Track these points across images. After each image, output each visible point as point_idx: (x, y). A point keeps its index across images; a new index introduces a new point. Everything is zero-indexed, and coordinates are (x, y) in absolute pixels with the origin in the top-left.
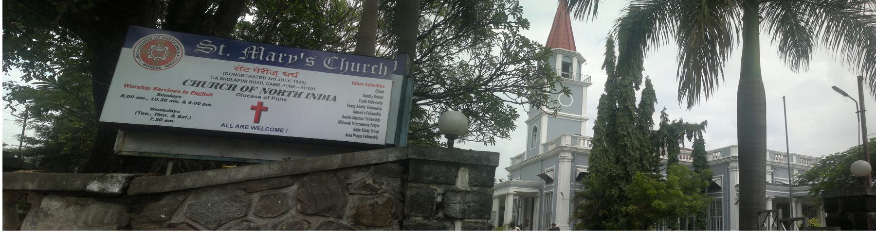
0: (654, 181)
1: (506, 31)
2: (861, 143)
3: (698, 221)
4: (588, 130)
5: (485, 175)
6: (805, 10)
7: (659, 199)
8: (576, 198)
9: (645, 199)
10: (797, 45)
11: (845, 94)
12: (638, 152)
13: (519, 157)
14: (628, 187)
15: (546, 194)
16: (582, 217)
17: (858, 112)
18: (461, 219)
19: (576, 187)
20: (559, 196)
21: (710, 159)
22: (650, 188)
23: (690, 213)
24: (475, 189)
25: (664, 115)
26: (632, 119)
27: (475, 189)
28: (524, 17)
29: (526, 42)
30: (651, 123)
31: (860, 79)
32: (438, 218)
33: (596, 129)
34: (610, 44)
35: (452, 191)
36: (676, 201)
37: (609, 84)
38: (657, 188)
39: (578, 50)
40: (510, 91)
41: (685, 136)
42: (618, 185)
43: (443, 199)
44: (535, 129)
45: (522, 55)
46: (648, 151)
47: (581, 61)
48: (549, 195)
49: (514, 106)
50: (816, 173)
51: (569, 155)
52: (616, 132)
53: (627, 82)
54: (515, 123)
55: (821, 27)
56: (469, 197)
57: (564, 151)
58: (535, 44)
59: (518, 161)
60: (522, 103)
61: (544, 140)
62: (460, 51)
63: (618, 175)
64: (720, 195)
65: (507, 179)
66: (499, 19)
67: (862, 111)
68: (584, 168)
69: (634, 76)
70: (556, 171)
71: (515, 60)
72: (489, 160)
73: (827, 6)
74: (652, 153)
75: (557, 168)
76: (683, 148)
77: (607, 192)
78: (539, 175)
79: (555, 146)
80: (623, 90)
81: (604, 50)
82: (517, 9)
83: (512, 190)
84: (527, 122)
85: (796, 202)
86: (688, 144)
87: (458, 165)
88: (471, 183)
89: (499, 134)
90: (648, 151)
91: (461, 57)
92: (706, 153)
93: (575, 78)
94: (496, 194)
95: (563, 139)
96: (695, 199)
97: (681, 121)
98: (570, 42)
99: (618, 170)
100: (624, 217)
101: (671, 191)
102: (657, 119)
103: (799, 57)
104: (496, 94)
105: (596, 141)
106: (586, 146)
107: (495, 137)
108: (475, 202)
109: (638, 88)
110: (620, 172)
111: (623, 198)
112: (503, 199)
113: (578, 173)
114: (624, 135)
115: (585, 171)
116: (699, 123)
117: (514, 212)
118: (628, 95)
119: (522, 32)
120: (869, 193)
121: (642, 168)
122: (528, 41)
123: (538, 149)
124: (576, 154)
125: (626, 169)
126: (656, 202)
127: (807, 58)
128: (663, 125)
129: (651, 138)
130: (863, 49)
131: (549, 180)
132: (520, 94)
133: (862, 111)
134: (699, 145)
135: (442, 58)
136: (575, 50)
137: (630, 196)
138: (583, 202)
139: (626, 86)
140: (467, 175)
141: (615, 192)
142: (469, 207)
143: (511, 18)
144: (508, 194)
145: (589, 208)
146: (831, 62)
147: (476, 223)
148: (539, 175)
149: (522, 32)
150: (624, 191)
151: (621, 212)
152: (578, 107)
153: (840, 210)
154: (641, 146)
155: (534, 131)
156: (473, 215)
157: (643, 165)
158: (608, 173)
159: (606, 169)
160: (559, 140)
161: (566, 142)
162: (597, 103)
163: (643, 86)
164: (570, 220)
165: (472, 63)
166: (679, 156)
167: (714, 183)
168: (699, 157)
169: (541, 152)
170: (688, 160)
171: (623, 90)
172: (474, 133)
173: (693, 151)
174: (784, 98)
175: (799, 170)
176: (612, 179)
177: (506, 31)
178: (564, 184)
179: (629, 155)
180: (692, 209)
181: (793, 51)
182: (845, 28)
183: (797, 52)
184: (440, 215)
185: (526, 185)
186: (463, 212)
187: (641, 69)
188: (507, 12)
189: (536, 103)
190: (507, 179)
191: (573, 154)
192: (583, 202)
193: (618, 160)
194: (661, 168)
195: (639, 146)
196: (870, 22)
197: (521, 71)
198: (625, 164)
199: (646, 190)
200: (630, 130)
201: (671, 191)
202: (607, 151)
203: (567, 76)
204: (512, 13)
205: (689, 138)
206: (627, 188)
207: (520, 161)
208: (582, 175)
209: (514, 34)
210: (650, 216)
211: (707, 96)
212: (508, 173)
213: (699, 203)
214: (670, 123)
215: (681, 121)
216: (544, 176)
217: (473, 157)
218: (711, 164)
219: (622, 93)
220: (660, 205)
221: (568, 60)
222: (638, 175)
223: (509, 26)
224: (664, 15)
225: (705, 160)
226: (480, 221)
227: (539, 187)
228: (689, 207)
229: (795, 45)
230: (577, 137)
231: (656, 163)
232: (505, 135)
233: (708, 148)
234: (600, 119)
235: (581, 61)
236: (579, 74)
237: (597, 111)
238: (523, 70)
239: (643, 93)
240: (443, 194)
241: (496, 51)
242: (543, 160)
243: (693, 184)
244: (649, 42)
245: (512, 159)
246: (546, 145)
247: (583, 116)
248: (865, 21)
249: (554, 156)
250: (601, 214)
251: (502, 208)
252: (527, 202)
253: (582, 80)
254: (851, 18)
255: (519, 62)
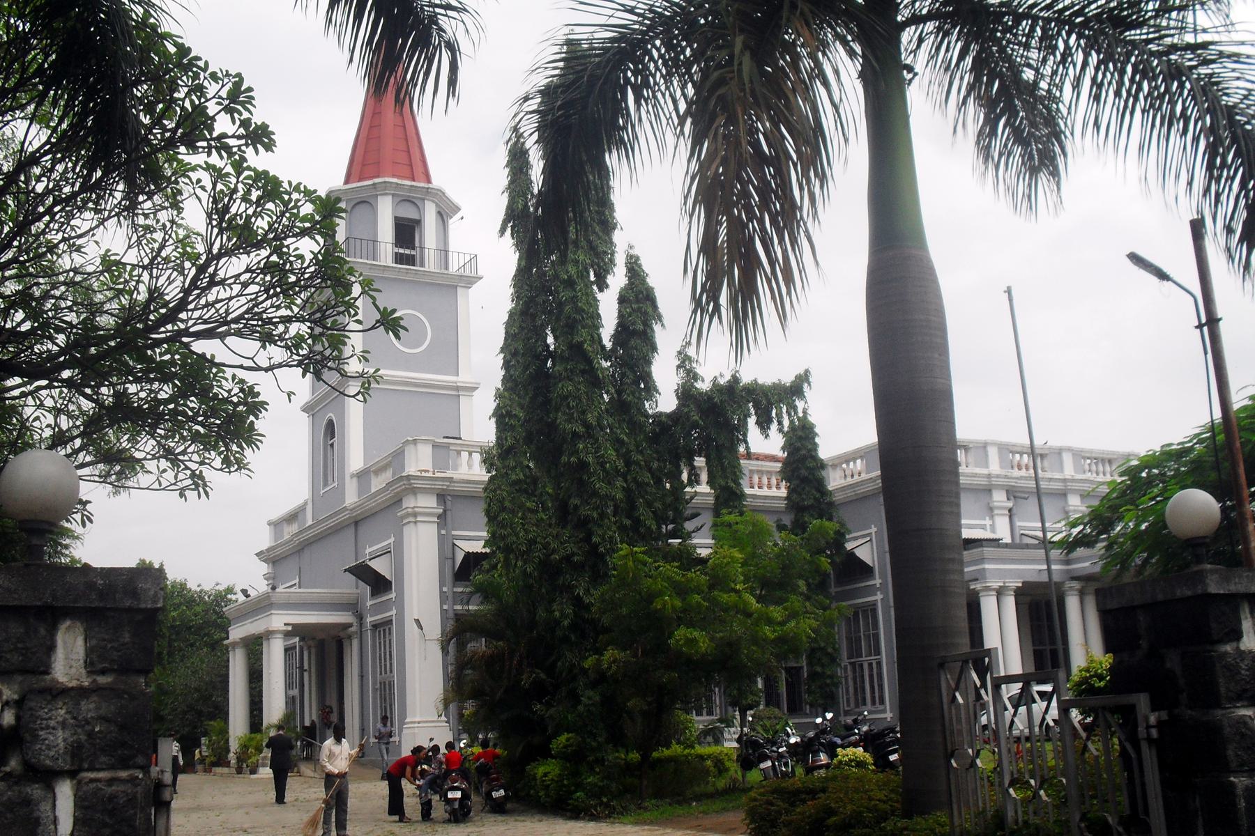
0: (671, 569)
1: (215, 159)
2: (1218, 414)
3: (813, 676)
4: (479, 424)
5: (127, 637)
6: (1030, 35)
7: (691, 625)
8: (459, 631)
9: (648, 627)
10: (1024, 128)
11: (1162, 276)
12: (620, 483)
13: (292, 517)
14: (596, 593)
15: (375, 626)
16: (476, 694)
17: (1200, 326)
18: (72, 774)
19: (457, 598)
20: (411, 629)
21: (835, 481)
22: (660, 594)
23: (781, 657)
24: (103, 680)
25: (684, 362)
26: (595, 380)
27: (103, 680)
28: (257, 119)
29: (270, 187)
30: (651, 390)
31: (1197, 228)
32: (9, 775)
33: (502, 417)
34: (518, 159)
35: (42, 691)
36: (738, 628)
37: (522, 278)
38: (681, 590)
39: (437, 181)
40: (239, 334)
41: (752, 421)
42: (569, 588)
43: (18, 718)
44: (330, 429)
45: (262, 224)
46: (647, 478)
47: (446, 211)
48: (383, 627)
49: (250, 378)
50: (1114, 508)
51: (428, 503)
52: (552, 426)
53: (572, 270)
54: (260, 425)
55: (1077, 85)
56: (88, 708)
57: (414, 491)
58: (297, 188)
59: (290, 531)
60: (270, 369)
61: (355, 459)
62: (102, 222)
63: (567, 558)
64: (872, 590)
65: (261, 587)
66: (195, 127)
67: (1211, 323)
68: (474, 541)
69: (592, 248)
70: (396, 553)
71: (246, 239)
72: (134, 594)
73: (1084, 25)
74: (659, 482)
75: (399, 543)
76: (749, 455)
77: (541, 614)
78: (350, 570)
79: (387, 476)
80: (564, 295)
81: (502, 177)
82: (238, 97)
83: (279, 621)
84: (307, 409)
85: (1082, 594)
86: (765, 442)
87: (52, 615)
88: (92, 665)
89: (218, 463)
90: (647, 478)
91: (99, 239)
92: (822, 465)
93: (431, 262)
94: (237, 633)
95: (410, 452)
96: (793, 615)
97: (735, 380)
98: (412, 160)
99: (565, 544)
100: (594, 685)
101: (725, 598)
102: (665, 377)
103: (1034, 171)
104: (199, 346)
105: (499, 457)
106: (473, 471)
107: (207, 473)
108: (103, 719)
109: (602, 286)
110: (571, 548)
111: (587, 631)
112: (254, 647)
113: (460, 557)
114: (575, 434)
115: (477, 547)
116: (788, 379)
117: (289, 685)
118: (579, 311)
119: (257, 159)
120: (1213, 589)
121: (635, 533)
122: (276, 182)
123: (341, 490)
124: (449, 497)
125: (588, 539)
126: (681, 633)
127: (1055, 173)
128: (686, 394)
129: (655, 439)
130: (1196, 140)
131: (379, 584)
132: (267, 339)
133: (1211, 323)
134: (801, 440)
135: (52, 248)
136: (429, 181)
137: (606, 620)
138: (479, 646)
139: (570, 283)
140: (80, 642)
141: (562, 611)
142: (91, 735)
143: (224, 125)
144: (268, 634)
145: (491, 664)
146: (1126, 177)
147: (111, 781)
148: (350, 570)
149: (257, 159)
150: (587, 607)
151: (584, 672)
152: (447, 350)
153: (1144, 643)
154: (628, 463)
155: (329, 434)
156: (103, 759)
157: (637, 522)
158: (537, 555)
159: (532, 542)
160: (399, 455)
161: (420, 461)
162: (499, 339)
163: (618, 280)
164: (446, 703)
165: (131, 257)
166: (744, 482)
167: (851, 555)
168: (804, 480)
169: (351, 497)
170: (774, 492)
171: (564, 295)
172: (151, 465)
173: (787, 463)
174: (1009, 291)
175: (1084, 496)
176: (550, 570)
177: (215, 159)
178: (423, 599)
179: (595, 493)
180: (787, 646)
181: (1016, 159)
182: (1139, 89)
183: (1027, 157)
184: (13, 764)
185: (316, 601)
186: (75, 751)
187: (608, 226)
188: (212, 108)
189: (320, 361)
190: (261, 587)
191: (442, 497)
192: (479, 646)
193: (564, 513)
194: (689, 526)
195: (620, 464)
196: (1206, 62)
197: (264, 271)
198: (584, 523)
199: (651, 597)
200: (591, 418)
201: (725, 598)
202: (535, 481)
203: (410, 260)
204: (227, 110)
205: (764, 424)
206: (594, 597)
207: (294, 528)
208: (472, 560)
209: (239, 166)
210: (666, 677)
211: (783, 317)
212: (264, 568)
213: (806, 626)
214: (704, 386)
215: (735, 380)
216: (363, 572)
217: (91, 586)
218: (838, 498)
219: (561, 305)
220: (692, 642)
221: (408, 213)
222: (624, 554)
223: (221, 145)
224: (642, 72)
225: (820, 485)
226: (124, 774)
227: (354, 607)
228: (781, 640)
229: (1019, 137)
230: (447, 447)
231: (676, 509)
232: (233, 463)
233: (826, 449)
234: (510, 381)
235: (446, 211)
236: (444, 252)
237: (500, 360)
238: (268, 268)
239: (622, 300)
240: (19, 704)
241: (195, 215)
242: (357, 522)
243: (784, 568)
244: (612, 159)
245: (276, 525)
246: (362, 476)
247: (464, 378)
248: (1189, 60)
249: (388, 508)
250: (526, 680)
251: (255, 677)
252: (322, 653)
253: (454, 267)
254: (1152, 54)
255: (258, 245)
